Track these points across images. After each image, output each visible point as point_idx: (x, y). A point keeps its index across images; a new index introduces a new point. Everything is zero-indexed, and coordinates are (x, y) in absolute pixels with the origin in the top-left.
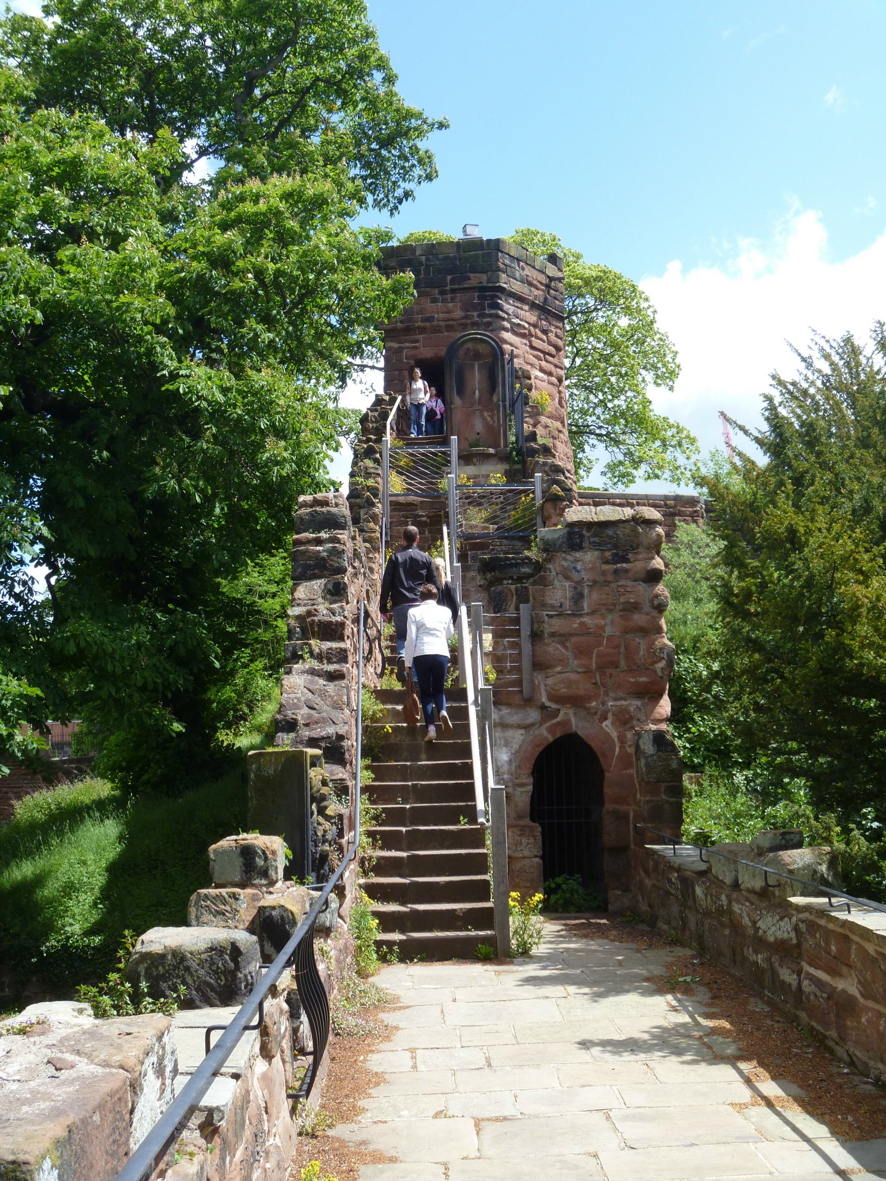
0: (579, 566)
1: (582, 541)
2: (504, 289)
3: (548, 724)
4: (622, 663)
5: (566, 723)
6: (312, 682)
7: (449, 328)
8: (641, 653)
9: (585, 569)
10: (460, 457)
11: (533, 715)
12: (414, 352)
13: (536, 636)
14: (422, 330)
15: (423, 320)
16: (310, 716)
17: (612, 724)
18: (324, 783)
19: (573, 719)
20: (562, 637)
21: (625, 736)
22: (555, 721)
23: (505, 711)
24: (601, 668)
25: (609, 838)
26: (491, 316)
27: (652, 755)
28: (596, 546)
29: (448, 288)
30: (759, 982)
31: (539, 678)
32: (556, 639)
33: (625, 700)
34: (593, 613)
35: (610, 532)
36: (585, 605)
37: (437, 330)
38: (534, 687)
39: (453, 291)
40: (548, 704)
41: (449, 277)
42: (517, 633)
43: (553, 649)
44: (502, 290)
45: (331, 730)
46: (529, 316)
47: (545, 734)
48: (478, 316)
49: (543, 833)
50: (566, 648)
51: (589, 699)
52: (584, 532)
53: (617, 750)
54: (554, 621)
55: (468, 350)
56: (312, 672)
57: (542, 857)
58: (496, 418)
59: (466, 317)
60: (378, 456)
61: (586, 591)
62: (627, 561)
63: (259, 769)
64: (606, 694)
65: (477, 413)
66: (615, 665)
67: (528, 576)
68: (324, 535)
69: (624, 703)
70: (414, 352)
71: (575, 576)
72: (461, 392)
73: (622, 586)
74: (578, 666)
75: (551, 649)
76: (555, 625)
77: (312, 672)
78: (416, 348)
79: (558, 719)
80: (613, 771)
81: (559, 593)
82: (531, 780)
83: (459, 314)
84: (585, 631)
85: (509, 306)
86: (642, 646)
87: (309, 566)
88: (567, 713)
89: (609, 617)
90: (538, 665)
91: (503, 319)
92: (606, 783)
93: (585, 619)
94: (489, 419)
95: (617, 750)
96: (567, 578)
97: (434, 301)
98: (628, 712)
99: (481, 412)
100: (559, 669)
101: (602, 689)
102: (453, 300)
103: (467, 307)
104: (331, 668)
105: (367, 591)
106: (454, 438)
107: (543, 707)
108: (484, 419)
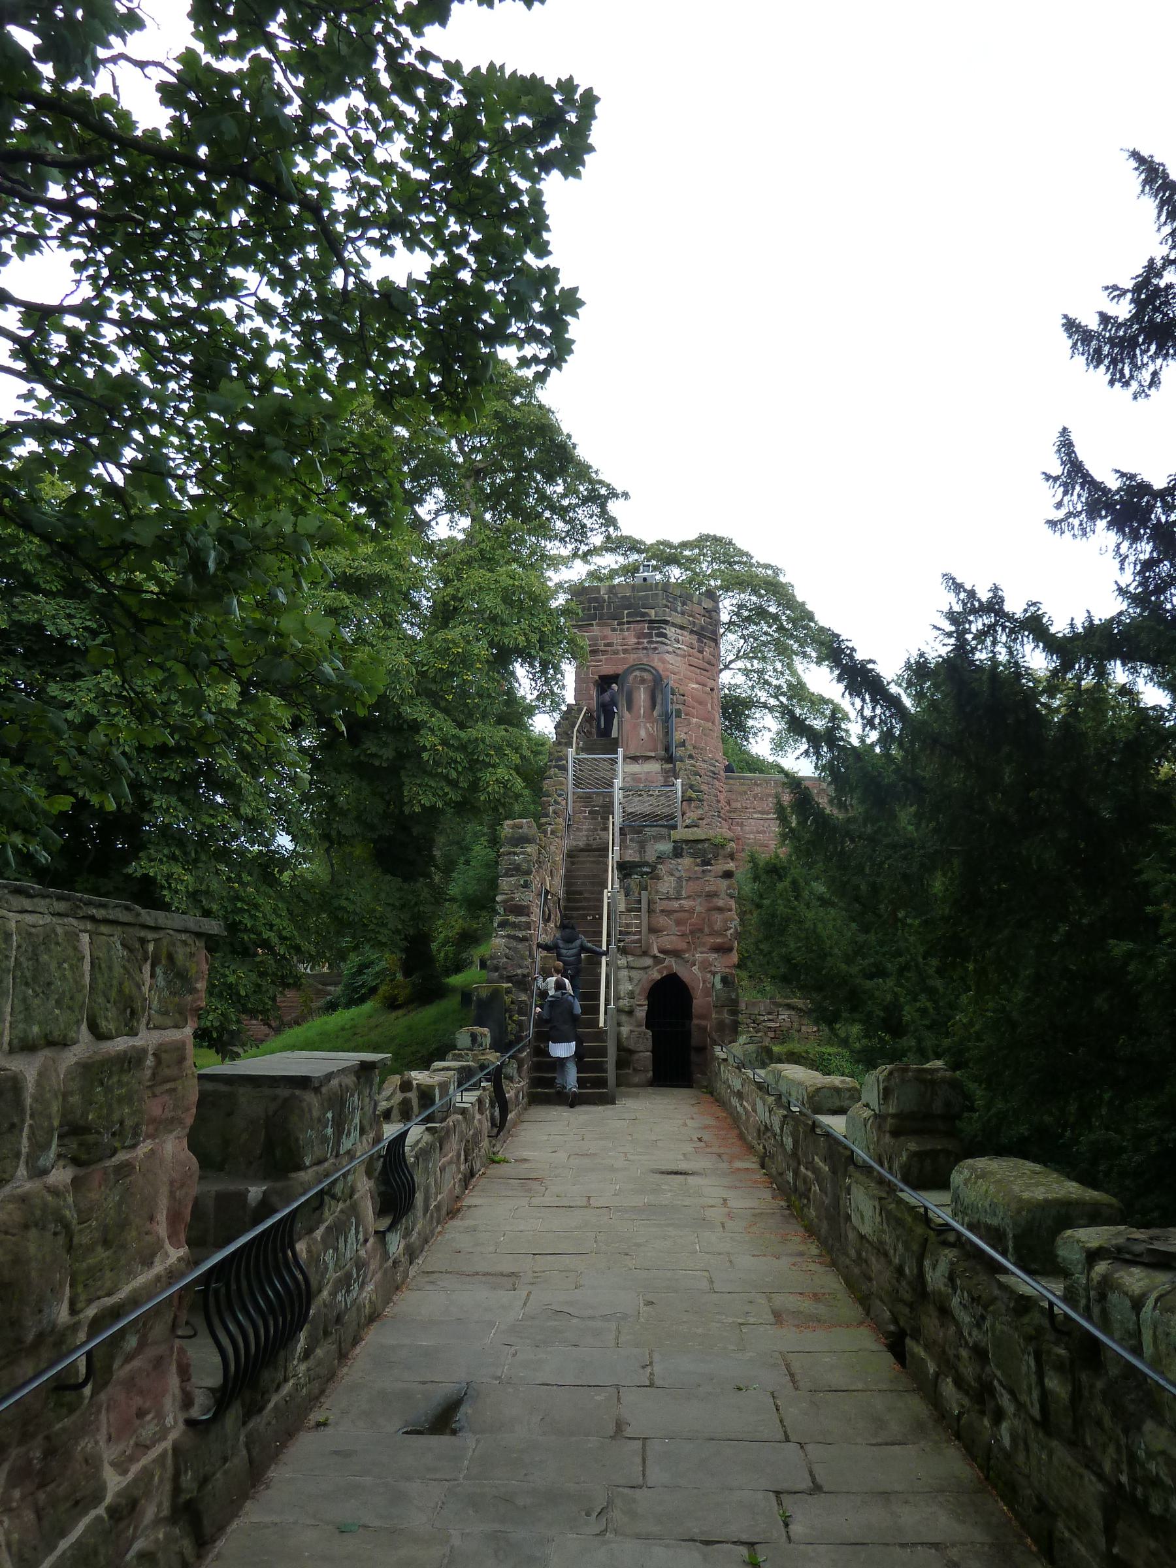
4: (706, 930)
5: (669, 967)
7: (625, 652)
10: (625, 758)
11: (648, 961)
12: (596, 669)
13: (650, 911)
15: (605, 645)
18: (512, 1002)
20: (667, 912)
23: (630, 958)
24: (692, 932)
25: (695, 1041)
26: (657, 642)
28: (691, 855)
30: (731, 1114)
31: (652, 938)
34: (689, 897)
35: (700, 846)
37: (616, 653)
38: (649, 946)
39: (629, 623)
42: (639, 910)
43: (663, 921)
44: (666, 622)
45: (519, 971)
46: (686, 637)
47: (656, 975)
51: (684, 951)
54: (666, 902)
56: (508, 936)
59: (638, 643)
62: (711, 865)
64: (695, 949)
66: (701, 930)
67: (647, 873)
68: (518, 850)
70: (596, 669)
72: (629, 708)
76: (666, 905)
77: (508, 936)
81: (667, 885)
84: (682, 909)
85: (670, 631)
88: (670, 961)
90: (653, 930)
97: (614, 630)
102: (628, 629)
103: (641, 635)
106: (620, 750)
107: (655, 957)
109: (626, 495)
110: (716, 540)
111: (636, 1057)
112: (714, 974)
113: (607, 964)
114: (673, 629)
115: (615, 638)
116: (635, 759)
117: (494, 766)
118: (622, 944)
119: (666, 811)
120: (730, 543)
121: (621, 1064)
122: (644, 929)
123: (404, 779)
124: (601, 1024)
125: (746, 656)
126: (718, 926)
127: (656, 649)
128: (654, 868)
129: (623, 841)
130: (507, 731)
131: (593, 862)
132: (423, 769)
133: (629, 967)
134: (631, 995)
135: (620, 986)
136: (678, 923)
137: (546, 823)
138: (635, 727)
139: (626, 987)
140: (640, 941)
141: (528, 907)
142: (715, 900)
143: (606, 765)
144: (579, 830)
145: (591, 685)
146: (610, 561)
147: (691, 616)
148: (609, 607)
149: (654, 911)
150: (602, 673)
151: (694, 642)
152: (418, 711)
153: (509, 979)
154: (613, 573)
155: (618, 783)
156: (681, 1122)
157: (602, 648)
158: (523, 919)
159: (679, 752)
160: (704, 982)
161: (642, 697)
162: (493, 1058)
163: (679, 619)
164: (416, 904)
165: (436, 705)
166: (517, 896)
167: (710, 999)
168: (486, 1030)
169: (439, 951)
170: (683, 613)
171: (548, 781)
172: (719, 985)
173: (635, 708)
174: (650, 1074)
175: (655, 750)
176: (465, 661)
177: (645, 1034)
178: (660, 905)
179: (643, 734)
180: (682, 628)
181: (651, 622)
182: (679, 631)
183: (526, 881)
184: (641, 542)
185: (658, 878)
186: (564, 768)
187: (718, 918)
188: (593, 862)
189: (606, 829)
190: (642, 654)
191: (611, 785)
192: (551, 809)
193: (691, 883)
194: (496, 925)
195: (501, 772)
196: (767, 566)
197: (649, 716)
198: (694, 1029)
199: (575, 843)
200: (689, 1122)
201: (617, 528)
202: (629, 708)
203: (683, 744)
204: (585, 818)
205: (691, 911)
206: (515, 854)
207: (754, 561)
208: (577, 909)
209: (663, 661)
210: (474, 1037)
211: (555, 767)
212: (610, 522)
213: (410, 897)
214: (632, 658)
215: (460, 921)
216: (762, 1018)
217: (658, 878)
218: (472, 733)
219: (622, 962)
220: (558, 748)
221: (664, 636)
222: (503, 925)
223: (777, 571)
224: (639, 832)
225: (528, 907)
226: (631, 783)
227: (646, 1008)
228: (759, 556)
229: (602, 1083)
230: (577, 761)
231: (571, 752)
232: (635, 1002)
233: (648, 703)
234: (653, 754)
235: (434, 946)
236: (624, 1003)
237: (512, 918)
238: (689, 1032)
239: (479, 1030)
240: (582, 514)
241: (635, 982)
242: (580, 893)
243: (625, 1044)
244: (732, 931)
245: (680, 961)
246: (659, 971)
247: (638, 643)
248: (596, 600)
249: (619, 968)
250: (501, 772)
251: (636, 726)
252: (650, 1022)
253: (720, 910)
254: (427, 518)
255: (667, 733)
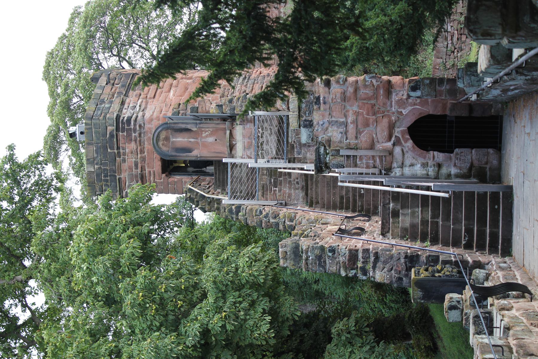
0: (322, 123)
1: (308, 121)
2: (117, 115)
3: (403, 142)
4: (373, 102)
5: (403, 133)
6: (379, 267)
7: (142, 152)
8: (367, 92)
9: (323, 119)
11: (398, 150)
14: (143, 169)
15: (137, 167)
16: (396, 270)
17: (404, 109)
19: (401, 129)
21: (411, 103)
22: (401, 138)
23: (395, 165)
24: (374, 114)
26: (135, 125)
27: (422, 93)
28: (311, 113)
29: (116, 151)
31: (379, 146)
32: (359, 136)
33: (392, 102)
34: (346, 116)
36: (342, 120)
37: (143, 159)
38: (385, 150)
39: (118, 148)
40: (392, 142)
41: (109, 150)
43: (364, 138)
44: (118, 117)
45: (402, 260)
46: (131, 100)
47: (410, 143)
48: (135, 133)
49: (459, 147)
50: (363, 131)
52: (303, 119)
53: (418, 107)
54: (349, 136)
55: (163, 145)
56: (374, 267)
57: (472, 148)
58: (207, 129)
59: (135, 141)
60: (233, 207)
61: (333, 119)
63: (420, 298)
65: (203, 140)
66: (373, 106)
67: (325, 149)
68: (304, 256)
69: (393, 103)
70: (157, 177)
71: (326, 125)
72: (189, 150)
73: (332, 100)
74: (373, 125)
75: (364, 139)
77: (374, 267)
78: (154, 172)
79: (400, 137)
80: (429, 110)
81: (335, 134)
82: (431, 152)
83: (133, 145)
84: (355, 122)
85: (126, 114)
86: (364, 91)
87: (319, 264)
88: (397, 132)
89: (348, 107)
90: (372, 147)
91: (137, 117)
92: (435, 113)
93: (349, 121)
94: (207, 133)
95: (418, 107)
96: (327, 129)
97: (124, 161)
98: (399, 100)
99: (202, 137)
100: (374, 136)
101: (386, 113)
102: (124, 149)
103: (129, 139)
104: (372, 259)
105: (322, 224)
106: (224, 160)
107: (394, 145)
108: (207, 136)
109: (11, 148)
110: (48, 65)
111: (476, 163)
112: (409, 96)
113: (399, 187)
114: (124, 111)
115: (131, 160)
116: (232, 147)
117: (237, 269)
118: (383, 172)
119: (275, 122)
120: (51, 54)
121: (482, 178)
122: (370, 153)
123: (247, 342)
124: (446, 195)
125: (147, 43)
126: (369, 92)
127: (140, 126)
128: (321, 144)
129: (300, 161)
130: (207, 256)
131: (316, 185)
132: (240, 328)
133: (402, 166)
134: (425, 165)
135: (418, 173)
136: (367, 125)
137: (284, 225)
138: (205, 145)
139: (418, 169)
140: (381, 157)
141: (350, 250)
142: (348, 94)
143: (236, 171)
144: (290, 196)
145: (170, 180)
146: (65, 157)
147: (113, 96)
148: (105, 165)
149: (356, 145)
150: (160, 171)
151: (135, 93)
152: (192, 330)
153: (409, 270)
154: (76, 153)
155: (252, 163)
156: (526, 137)
157: (139, 170)
158: (360, 255)
159: (227, 111)
160: (415, 104)
161: (180, 140)
162: (468, 292)
163: (116, 106)
164: (349, 333)
165: (186, 314)
166: (341, 259)
167: (430, 100)
168: (448, 296)
169: (390, 308)
170: (111, 102)
171: (249, 222)
172: (418, 93)
173: (189, 146)
174: (491, 151)
175: (225, 130)
176: (150, 288)
177: (457, 154)
178: (353, 142)
179: (211, 139)
180: (123, 103)
181: (117, 129)
182: (126, 106)
183: (330, 251)
184: (50, 131)
185: (329, 141)
186: (239, 208)
187: (363, 92)
188: (316, 185)
189: (290, 174)
190: (145, 138)
191: (253, 169)
192: (272, 220)
193: (334, 114)
194: (364, 278)
195: (242, 262)
196: (72, 21)
197: (197, 134)
198: (454, 114)
199: (301, 200)
200: (528, 130)
201: (38, 155)
202: (189, 150)
203: (220, 106)
204: (280, 191)
205: (357, 114)
206: (307, 259)
207: (67, 34)
208: (355, 201)
209: (151, 120)
210: (452, 308)
211: (237, 215)
212: (34, 161)
213: (343, 338)
214: (148, 146)
215: (365, 289)
216: (450, 45)
217: (329, 141)
218: (209, 286)
219: (397, 172)
220: (222, 210)
221: (129, 119)
222: (365, 272)
223: (76, 14)
224: (293, 147)
225: (350, 250)
226: (252, 150)
227: (436, 153)
228: (62, 28)
229: (495, 196)
230: (234, 196)
231: (226, 200)
232: (430, 163)
233: (185, 134)
234: (228, 132)
235: (387, 313)
236: (431, 171)
237: (360, 264)
238: (456, 117)
239: (446, 304)
240: (29, 183)
241: (414, 161)
242: (342, 198)
243: (465, 171)
244: (374, 81)
245: (398, 124)
246: (406, 141)
247: (135, 141)
248: (98, 175)
249: (403, 175)
250: (242, 262)
251: (206, 145)
252: (447, 149)
253: (356, 90)
254: (28, 314)
255: (210, 118)
